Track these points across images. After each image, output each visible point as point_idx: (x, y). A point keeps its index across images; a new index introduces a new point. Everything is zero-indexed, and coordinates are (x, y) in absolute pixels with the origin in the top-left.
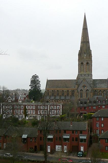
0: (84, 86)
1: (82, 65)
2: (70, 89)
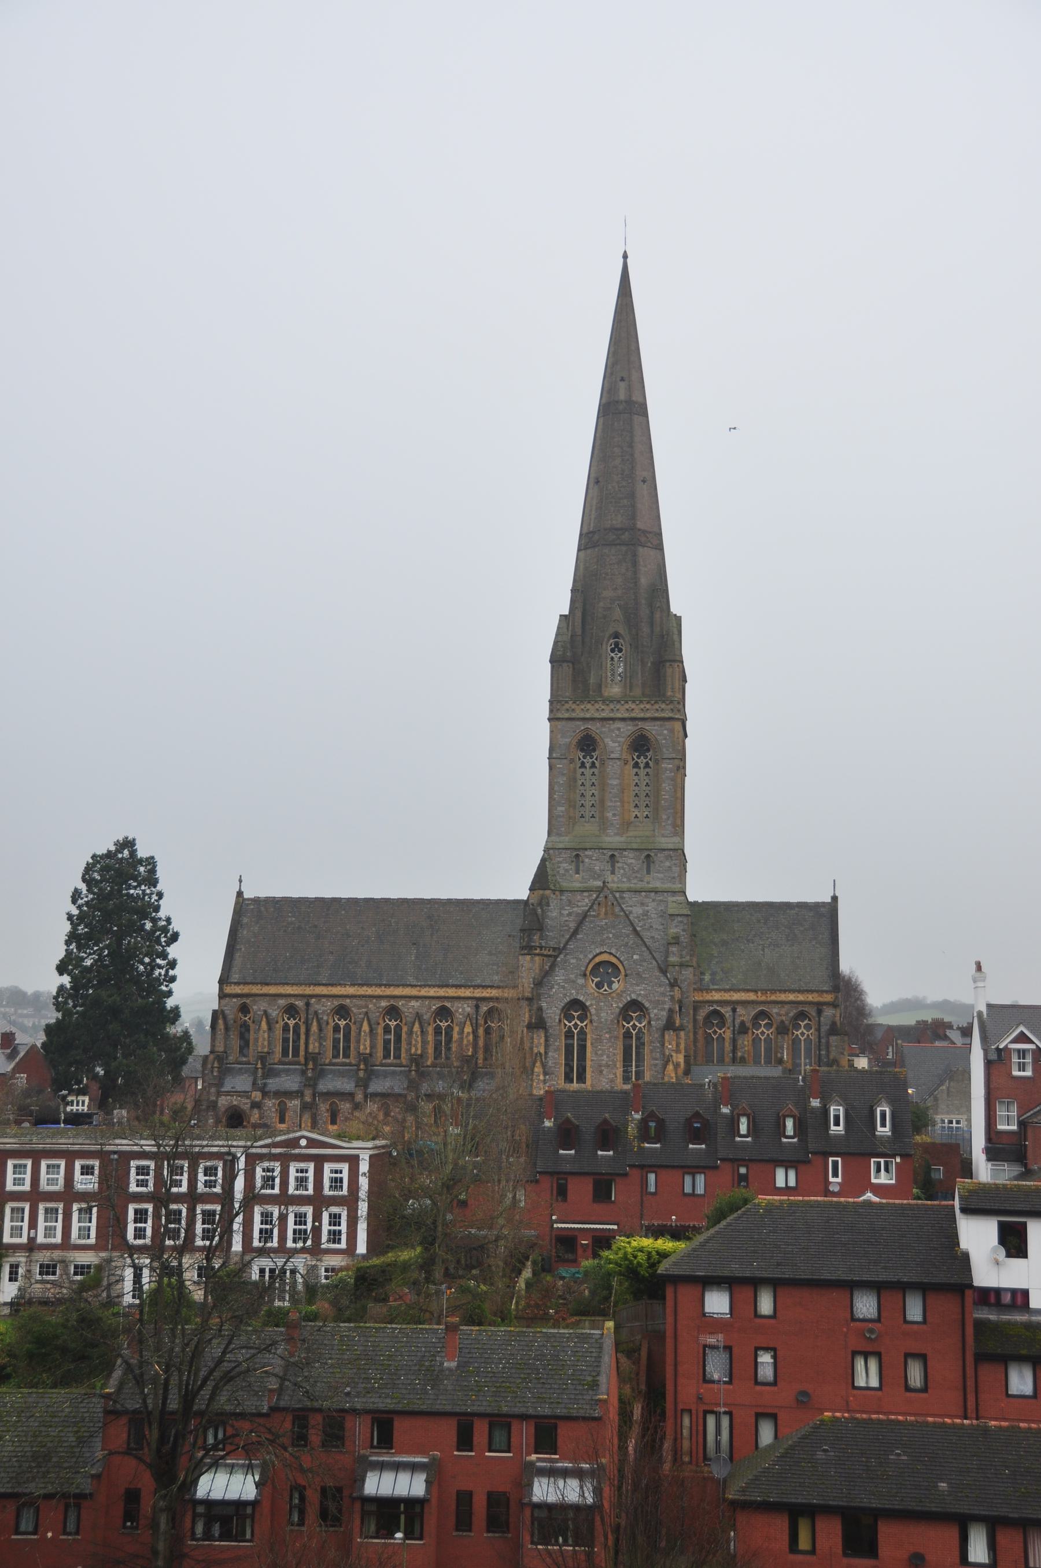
0: (604, 971)
1: (588, 761)
2: (468, 993)
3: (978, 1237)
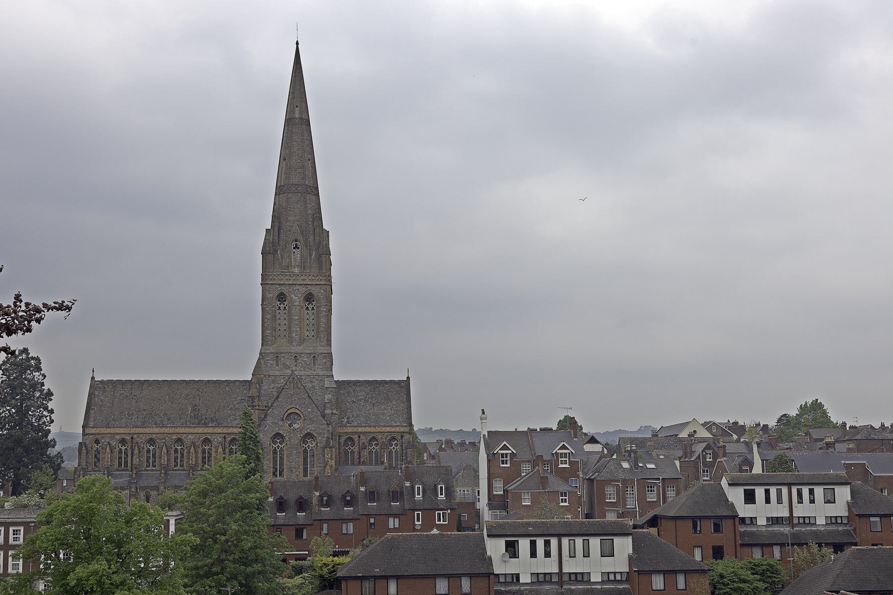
0: (291, 416)
2: (220, 430)
3: (495, 548)
